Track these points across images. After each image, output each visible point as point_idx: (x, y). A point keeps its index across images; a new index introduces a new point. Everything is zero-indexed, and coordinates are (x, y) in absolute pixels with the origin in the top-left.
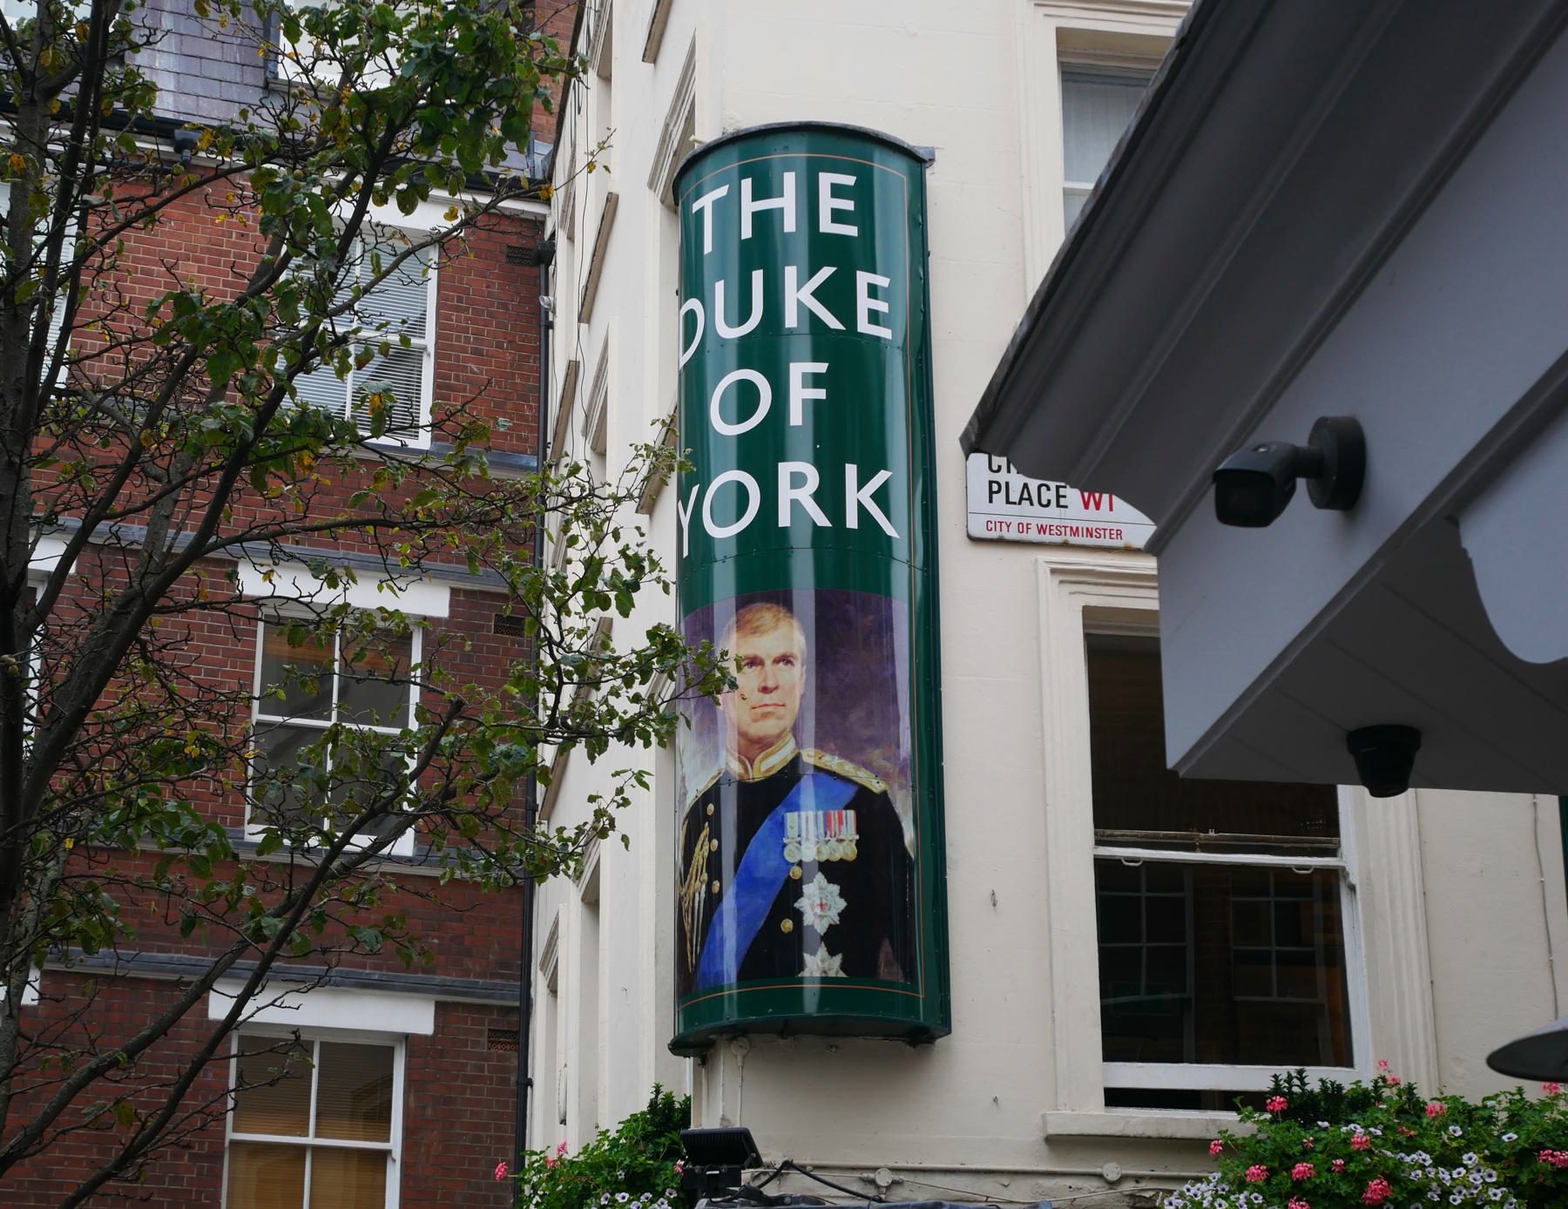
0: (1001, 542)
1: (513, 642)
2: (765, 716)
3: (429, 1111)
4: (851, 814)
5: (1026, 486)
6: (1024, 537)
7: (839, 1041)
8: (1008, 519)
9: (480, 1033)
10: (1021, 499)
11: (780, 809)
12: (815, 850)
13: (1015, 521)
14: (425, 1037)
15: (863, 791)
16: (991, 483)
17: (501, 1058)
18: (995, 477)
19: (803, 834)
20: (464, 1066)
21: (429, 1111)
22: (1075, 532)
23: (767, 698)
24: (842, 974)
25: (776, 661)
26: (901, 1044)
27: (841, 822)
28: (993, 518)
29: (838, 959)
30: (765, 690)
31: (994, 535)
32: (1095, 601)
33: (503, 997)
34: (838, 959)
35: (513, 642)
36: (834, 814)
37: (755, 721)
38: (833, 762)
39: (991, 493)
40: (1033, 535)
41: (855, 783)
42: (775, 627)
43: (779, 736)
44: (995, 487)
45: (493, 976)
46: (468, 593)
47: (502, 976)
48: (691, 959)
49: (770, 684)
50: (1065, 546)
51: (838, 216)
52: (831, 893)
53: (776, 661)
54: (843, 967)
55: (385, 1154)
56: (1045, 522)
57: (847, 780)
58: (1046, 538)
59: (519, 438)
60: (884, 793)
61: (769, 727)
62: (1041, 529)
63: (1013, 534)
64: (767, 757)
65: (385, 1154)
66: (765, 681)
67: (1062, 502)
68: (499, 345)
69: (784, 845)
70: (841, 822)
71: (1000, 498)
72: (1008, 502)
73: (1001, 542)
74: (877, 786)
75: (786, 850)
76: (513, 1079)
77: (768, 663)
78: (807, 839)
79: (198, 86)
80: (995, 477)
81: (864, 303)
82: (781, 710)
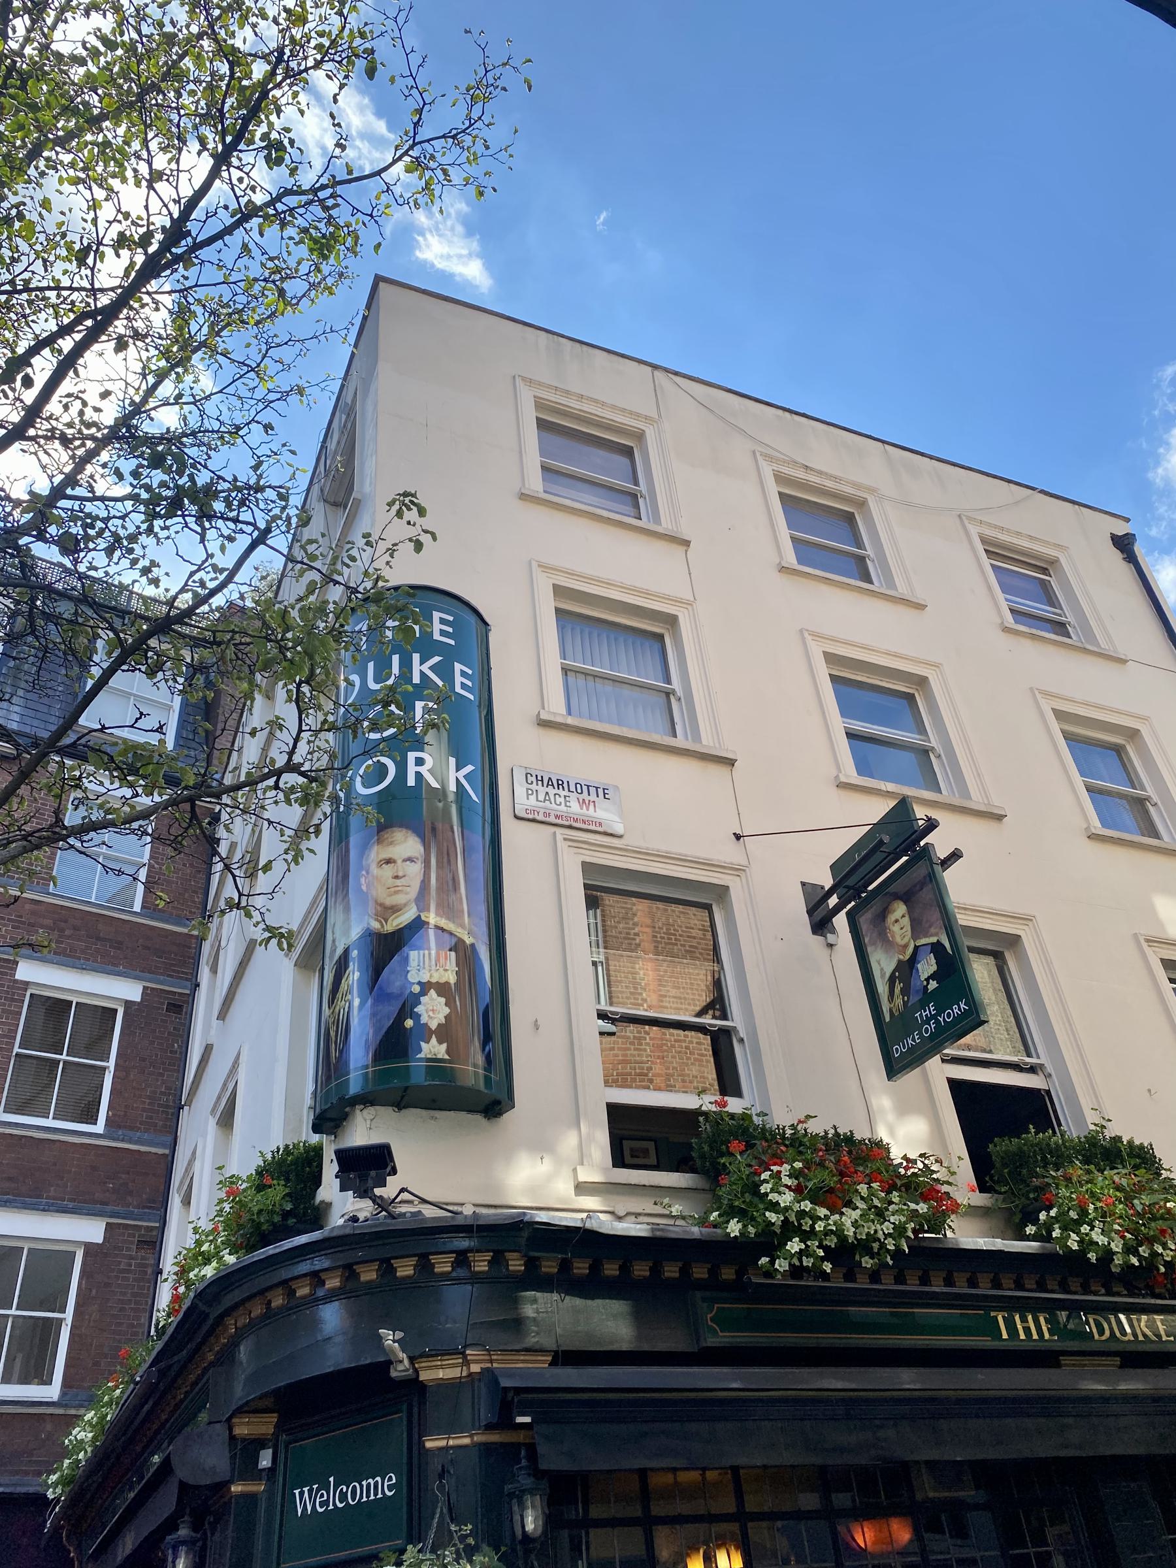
0: (534, 821)
1: (176, 1018)
2: (396, 892)
3: (94, 1292)
4: (453, 954)
5: (547, 793)
6: (547, 819)
7: (437, 1114)
8: (538, 810)
9: (132, 1243)
10: (545, 800)
11: (405, 949)
12: (429, 975)
13: (542, 811)
14: (98, 1244)
15: (460, 941)
16: (528, 789)
17: (143, 1258)
18: (530, 786)
19: (421, 964)
20: (120, 1262)
21: (94, 1292)
22: (576, 820)
23: (398, 882)
24: (447, 1057)
25: (405, 860)
26: (479, 1118)
27: (446, 958)
28: (529, 808)
29: (444, 1046)
30: (396, 877)
31: (530, 816)
32: (588, 859)
33: (149, 1220)
34: (444, 1046)
35: (176, 1018)
36: (442, 954)
37: (390, 895)
38: (443, 923)
39: (528, 795)
40: (552, 819)
41: (455, 936)
42: (405, 841)
43: (405, 905)
44: (530, 792)
45: (144, 1207)
46: (152, 989)
47: (150, 1208)
48: (334, 1054)
49: (400, 874)
50: (570, 827)
51: (443, 633)
52: (440, 1003)
53: (405, 860)
54: (448, 1052)
55: (104, 1069)
56: (559, 814)
57: (451, 934)
58: (559, 821)
59: (190, 912)
60: (473, 945)
61: (399, 899)
62: (557, 817)
63: (540, 817)
64: (396, 918)
65: (104, 1069)
66: (397, 872)
67: (568, 804)
68: (184, 865)
69: (408, 972)
70: (446, 958)
71: (533, 798)
72: (537, 800)
73: (534, 821)
74: (469, 941)
75: (409, 975)
76: (149, 1271)
77: (399, 862)
78: (424, 968)
79: (28, 721)
80: (530, 786)
81: (458, 679)
82: (408, 889)
